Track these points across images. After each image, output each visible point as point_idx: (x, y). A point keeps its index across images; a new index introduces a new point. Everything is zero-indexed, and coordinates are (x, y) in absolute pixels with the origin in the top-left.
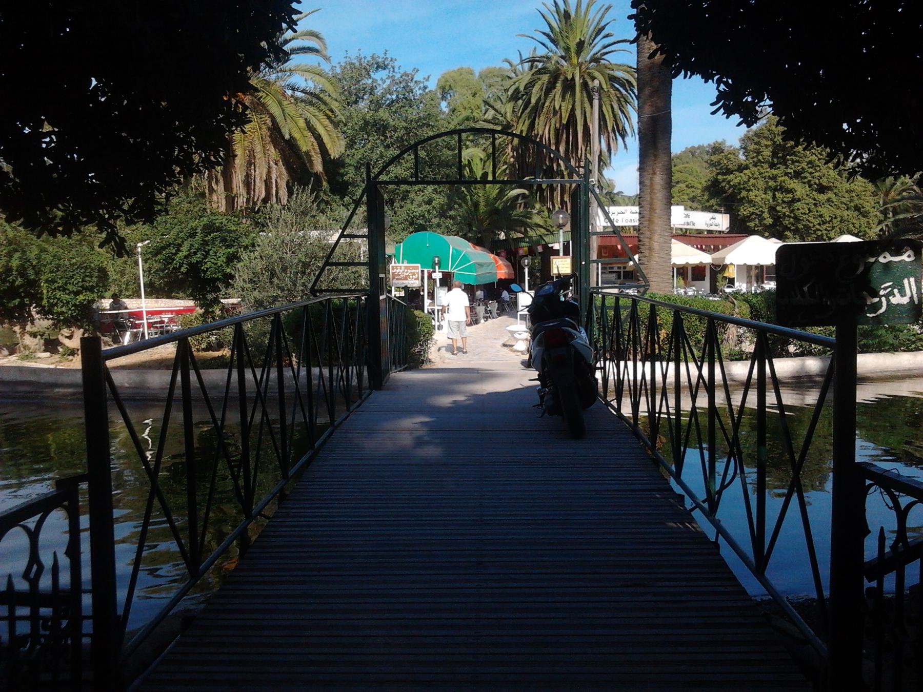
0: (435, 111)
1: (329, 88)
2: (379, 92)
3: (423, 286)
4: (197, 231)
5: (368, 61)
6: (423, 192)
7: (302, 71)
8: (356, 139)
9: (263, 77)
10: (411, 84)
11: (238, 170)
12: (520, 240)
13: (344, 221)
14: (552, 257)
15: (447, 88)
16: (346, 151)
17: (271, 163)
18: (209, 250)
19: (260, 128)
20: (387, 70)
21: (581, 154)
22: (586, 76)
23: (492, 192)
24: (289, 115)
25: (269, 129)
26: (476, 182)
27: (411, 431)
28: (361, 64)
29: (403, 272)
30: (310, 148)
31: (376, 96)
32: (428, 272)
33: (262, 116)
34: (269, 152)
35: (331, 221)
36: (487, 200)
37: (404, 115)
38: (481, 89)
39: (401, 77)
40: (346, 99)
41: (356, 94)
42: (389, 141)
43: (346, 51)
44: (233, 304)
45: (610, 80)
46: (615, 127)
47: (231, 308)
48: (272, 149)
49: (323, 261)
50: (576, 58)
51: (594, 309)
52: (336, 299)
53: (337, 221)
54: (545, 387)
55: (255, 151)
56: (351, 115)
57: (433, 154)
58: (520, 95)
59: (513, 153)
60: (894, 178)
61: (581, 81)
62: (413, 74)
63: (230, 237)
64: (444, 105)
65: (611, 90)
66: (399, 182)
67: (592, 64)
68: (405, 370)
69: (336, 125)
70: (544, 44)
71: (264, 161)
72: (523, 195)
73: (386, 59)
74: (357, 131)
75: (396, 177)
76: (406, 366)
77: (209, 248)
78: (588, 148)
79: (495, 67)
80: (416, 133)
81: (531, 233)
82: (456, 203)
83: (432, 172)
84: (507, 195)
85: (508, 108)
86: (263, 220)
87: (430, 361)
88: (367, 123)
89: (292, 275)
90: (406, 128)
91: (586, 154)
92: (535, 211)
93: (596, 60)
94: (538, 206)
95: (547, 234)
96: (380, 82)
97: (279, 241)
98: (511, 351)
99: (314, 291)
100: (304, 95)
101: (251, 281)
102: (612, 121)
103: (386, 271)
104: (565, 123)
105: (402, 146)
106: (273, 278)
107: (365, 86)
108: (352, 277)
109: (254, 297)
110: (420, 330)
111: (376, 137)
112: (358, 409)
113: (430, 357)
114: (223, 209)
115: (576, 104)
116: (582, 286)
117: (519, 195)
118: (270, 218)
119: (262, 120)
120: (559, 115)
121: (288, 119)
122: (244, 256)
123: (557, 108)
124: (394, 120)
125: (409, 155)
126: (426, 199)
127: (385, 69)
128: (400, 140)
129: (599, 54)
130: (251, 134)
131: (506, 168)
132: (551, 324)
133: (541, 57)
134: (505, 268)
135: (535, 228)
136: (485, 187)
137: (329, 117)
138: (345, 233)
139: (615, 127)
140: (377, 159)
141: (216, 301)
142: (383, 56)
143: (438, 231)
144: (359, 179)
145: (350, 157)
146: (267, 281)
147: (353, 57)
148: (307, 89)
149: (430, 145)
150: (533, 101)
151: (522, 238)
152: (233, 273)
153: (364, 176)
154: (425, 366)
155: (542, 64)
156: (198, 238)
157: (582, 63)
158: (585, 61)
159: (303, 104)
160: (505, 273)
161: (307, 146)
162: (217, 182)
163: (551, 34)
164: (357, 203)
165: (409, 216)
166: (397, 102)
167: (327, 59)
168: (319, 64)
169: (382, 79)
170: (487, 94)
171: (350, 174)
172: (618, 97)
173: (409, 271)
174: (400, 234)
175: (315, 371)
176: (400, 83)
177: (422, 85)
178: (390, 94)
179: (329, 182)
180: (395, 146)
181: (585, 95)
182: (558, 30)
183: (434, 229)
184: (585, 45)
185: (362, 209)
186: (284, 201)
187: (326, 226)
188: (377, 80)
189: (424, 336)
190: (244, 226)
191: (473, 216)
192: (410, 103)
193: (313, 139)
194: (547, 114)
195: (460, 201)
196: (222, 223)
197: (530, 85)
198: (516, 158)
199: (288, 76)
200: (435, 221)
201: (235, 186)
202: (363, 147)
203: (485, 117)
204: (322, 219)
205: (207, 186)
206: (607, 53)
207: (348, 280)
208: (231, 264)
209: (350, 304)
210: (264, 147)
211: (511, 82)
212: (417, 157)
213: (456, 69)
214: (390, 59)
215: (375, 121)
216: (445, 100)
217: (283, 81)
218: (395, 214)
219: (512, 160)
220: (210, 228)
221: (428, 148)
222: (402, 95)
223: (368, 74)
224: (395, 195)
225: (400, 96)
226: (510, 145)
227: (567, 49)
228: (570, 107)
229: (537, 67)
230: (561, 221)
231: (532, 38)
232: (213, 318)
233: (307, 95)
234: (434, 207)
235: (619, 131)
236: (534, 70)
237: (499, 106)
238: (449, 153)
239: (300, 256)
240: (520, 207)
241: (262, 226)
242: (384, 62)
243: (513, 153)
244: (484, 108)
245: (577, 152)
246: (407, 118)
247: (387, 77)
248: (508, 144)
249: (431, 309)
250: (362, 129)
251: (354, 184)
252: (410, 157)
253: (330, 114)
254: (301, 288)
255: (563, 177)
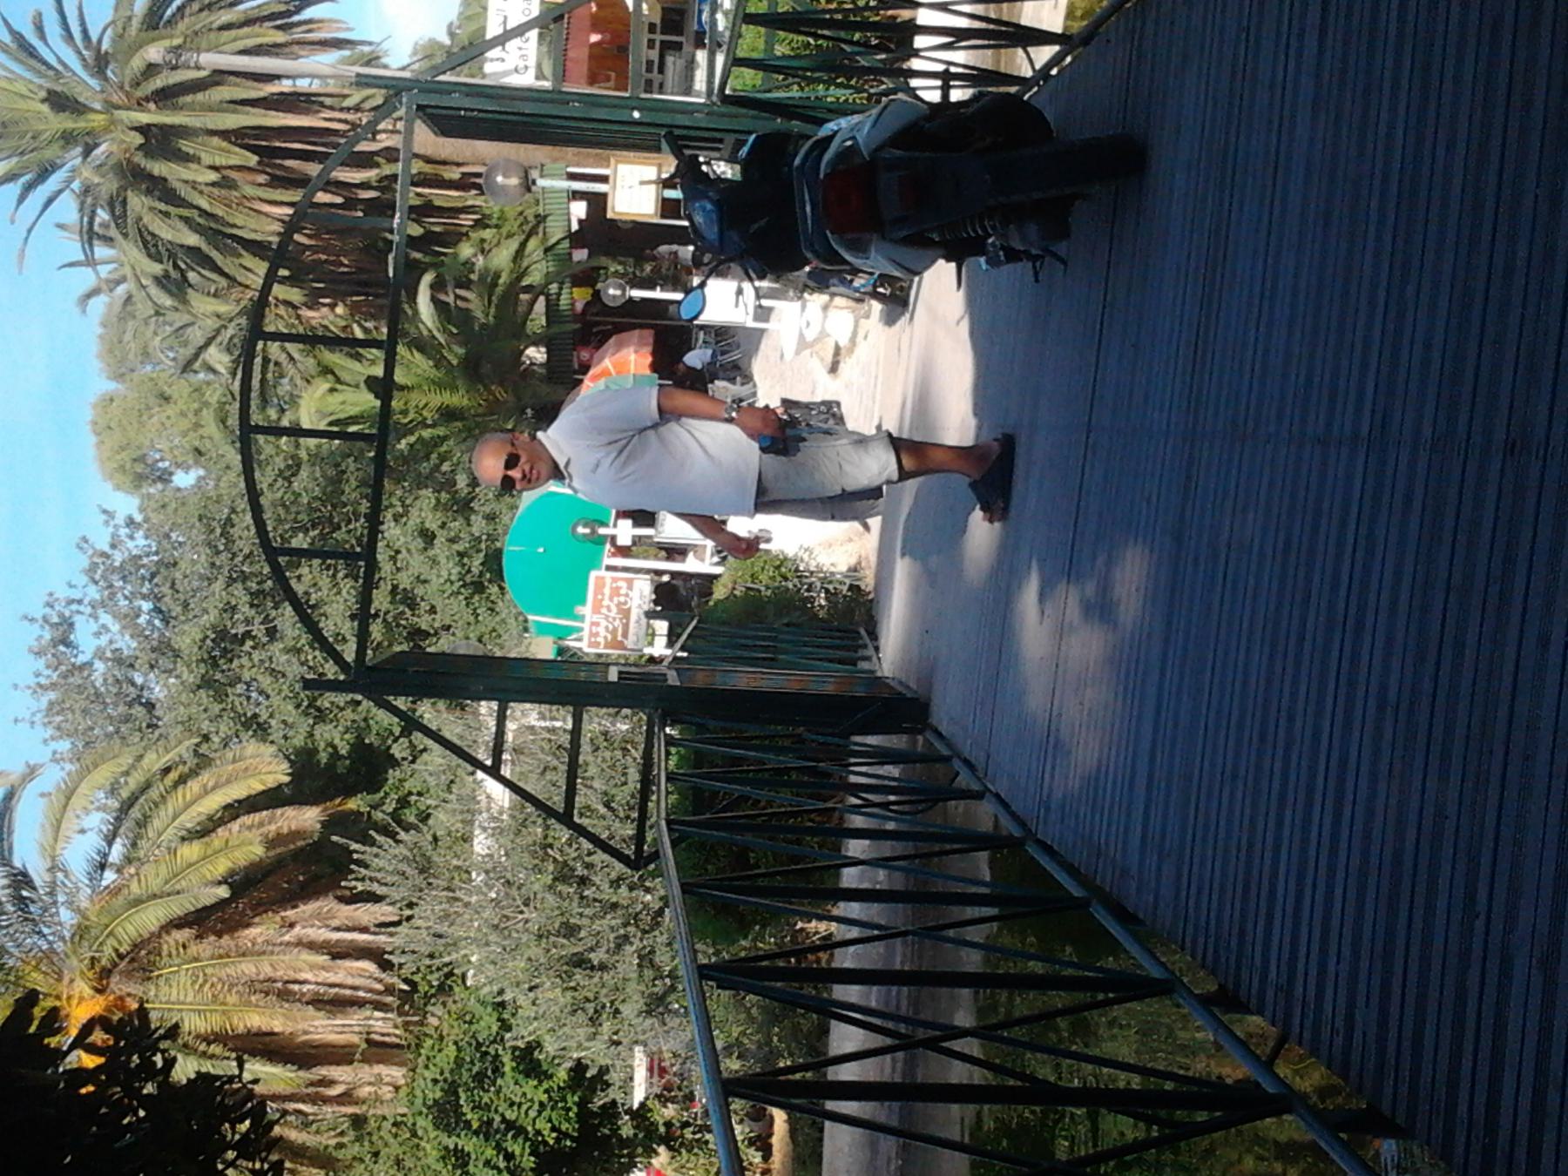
0: (193, 510)
1: (104, 774)
2: (127, 644)
3: (648, 571)
4: (452, 1147)
5: (48, 667)
6: (398, 552)
7: (56, 840)
8: (245, 714)
9: (65, 942)
10: (118, 558)
11: (301, 1026)
12: (552, 308)
13: (454, 764)
14: (610, 215)
15: (139, 468)
16: (272, 742)
17: (287, 938)
18: (504, 1120)
19: (196, 960)
20: (77, 619)
21: (340, 121)
22: (139, 93)
23: (419, 371)
24: (167, 882)
25: (199, 937)
26: (386, 410)
27: (1061, 632)
28: (53, 686)
29: (607, 617)
30: (255, 836)
31: (138, 653)
32: (614, 555)
33: (165, 953)
34: (259, 940)
35: (453, 797)
36: (440, 385)
37: (196, 584)
38: (152, 379)
39: (96, 583)
40: (140, 730)
41: (130, 705)
42: (258, 630)
43: (16, 721)
44: (650, 1069)
45: (156, 28)
46: (279, 22)
47: (662, 1077)
48: (252, 932)
49: (558, 826)
50: (92, 116)
51: (768, 95)
52: (663, 801)
53: (452, 782)
54: (984, 244)
55: (254, 977)
56: (182, 723)
57: (303, 517)
58: (174, 274)
59: (324, 305)
60: (141, 145)
61: (152, 106)
62: (90, 552)
63: (472, 1062)
64: (184, 480)
65: (181, 26)
66: (363, 616)
67: (109, 73)
68: (874, 635)
69: (203, 762)
70: (50, 201)
71: (282, 957)
72: (438, 286)
73: (45, 619)
74: (224, 710)
75: (353, 617)
76: (863, 632)
77: (498, 1119)
78: (328, 101)
79: (101, 337)
80: (247, 557)
81: (534, 277)
82: (437, 467)
83: (349, 522)
84: (430, 331)
85: (203, 305)
86: (436, 975)
87: (854, 569)
88: (206, 683)
89: (588, 911)
90: (231, 581)
91: (342, 110)
92: (480, 261)
93: (100, 64)
94: (466, 250)
95: (545, 233)
96: (104, 640)
97: (493, 938)
98: (851, 349)
99: (640, 860)
100: (118, 840)
101: (594, 1021)
102: (261, 30)
103: (601, 664)
104: (256, 158)
105: (274, 597)
106: (590, 961)
107: (110, 681)
108: (608, 754)
109: (638, 1016)
110: (767, 588)
111: (245, 661)
112: (980, 766)
113: (843, 568)
114: (396, 1073)
115: (211, 126)
116: (703, 125)
117: (434, 300)
118: (431, 956)
119: (174, 952)
120: (233, 175)
121: (178, 887)
122: (523, 1033)
123: (213, 176)
124: (206, 611)
125: (299, 578)
126: (420, 543)
127: (71, 625)
128: (257, 598)
129: (84, 52)
130: (208, 985)
131: (360, 325)
132: (808, 209)
133: (81, 210)
134: (624, 352)
135: (525, 264)
136: (402, 388)
137: (182, 780)
138: (489, 763)
139: (279, 22)
140: (302, 664)
141: (641, 1115)
142: (36, 626)
143: (506, 519)
144: (349, 714)
145: (291, 734)
146: (596, 980)
147: (34, 706)
148: (105, 830)
149: (280, 521)
150: (192, 239)
151: (548, 300)
152: (569, 1064)
153: (341, 699)
154: (868, 583)
155: (99, 211)
156: (469, 1144)
157: (106, 101)
158: (102, 92)
159: (142, 843)
160: (636, 352)
161: (251, 844)
162: (329, 1083)
163: (23, 180)
164: (412, 724)
165: (459, 593)
166: (159, 600)
167: (31, 772)
168: (43, 795)
169: (97, 634)
170: (168, 361)
171: (334, 737)
172: (201, 10)
173: (606, 602)
174: (503, 621)
175: (850, 878)
176: (111, 586)
177: (123, 531)
178: (138, 616)
179: (350, 792)
180: (273, 613)
181: (188, 98)
182: (15, 160)
183: (500, 531)
184: (59, 89)
185: (429, 712)
186: (384, 912)
187: (462, 812)
188: (98, 648)
189: (786, 579)
190: (445, 1025)
191: (477, 425)
192: (167, 566)
193: (235, 826)
194: (230, 207)
195: (434, 456)
196: (435, 1081)
197: (151, 245)
198: (338, 296)
199: (66, 876)
200: (479, 525)
201: (343, 1036)
202: (268, 697)
203: (223, 371)
204: (443, 820)
205: (337, 1108)
206: (85, 32)
207: (612, 767)
208: (545, 1067)
209: (678, 766)
210: (244, 955)
211: (139, 296)
212: (308, 554)
213: (93, 439)
214: (48, 610)
215: (203, 660)
216: (171, 474)
217: (78, 889)
218: (448, 628)
219: (340, 310)
220: (446, 1114)
221: (287, 527)
222: (142, 585)
223: (82, 668)
224: (398, 625)
225: (144, 590)
226: (300, 312)
227: (68, 138)
228: (216, 141)
229: (104, 225)
230: (514, 181)
231: (29, 231)
232: (686, 1125)
233: (122, 830)
234: (443, 526)
235: (289, 14)
236: (113, 232)
237: (199, 333)
238: (304, 473)
239: (536, 887)
240: (465, 299)
241: (449, 981)
242: (54, 626)
243: (324, 305)
244: (201, 376)
245: (335, 132)
246: (202, 577)
247: (91, 620)
248: (298, 317)
249: (712, 555)
250: (220, 696)
251: (361, 729)
252: (308, 578)
253: (173, 775)
254: (623, 890)
255: (394, 177)
